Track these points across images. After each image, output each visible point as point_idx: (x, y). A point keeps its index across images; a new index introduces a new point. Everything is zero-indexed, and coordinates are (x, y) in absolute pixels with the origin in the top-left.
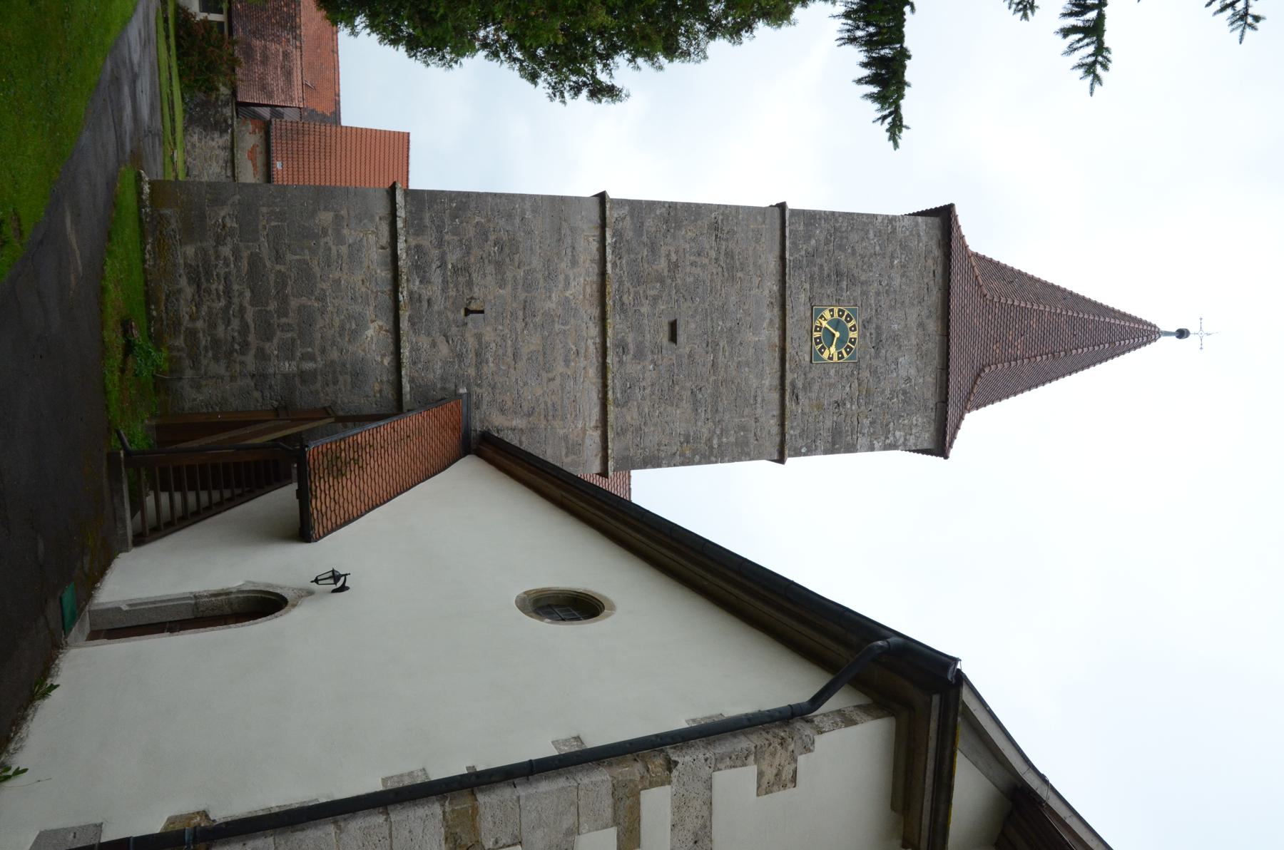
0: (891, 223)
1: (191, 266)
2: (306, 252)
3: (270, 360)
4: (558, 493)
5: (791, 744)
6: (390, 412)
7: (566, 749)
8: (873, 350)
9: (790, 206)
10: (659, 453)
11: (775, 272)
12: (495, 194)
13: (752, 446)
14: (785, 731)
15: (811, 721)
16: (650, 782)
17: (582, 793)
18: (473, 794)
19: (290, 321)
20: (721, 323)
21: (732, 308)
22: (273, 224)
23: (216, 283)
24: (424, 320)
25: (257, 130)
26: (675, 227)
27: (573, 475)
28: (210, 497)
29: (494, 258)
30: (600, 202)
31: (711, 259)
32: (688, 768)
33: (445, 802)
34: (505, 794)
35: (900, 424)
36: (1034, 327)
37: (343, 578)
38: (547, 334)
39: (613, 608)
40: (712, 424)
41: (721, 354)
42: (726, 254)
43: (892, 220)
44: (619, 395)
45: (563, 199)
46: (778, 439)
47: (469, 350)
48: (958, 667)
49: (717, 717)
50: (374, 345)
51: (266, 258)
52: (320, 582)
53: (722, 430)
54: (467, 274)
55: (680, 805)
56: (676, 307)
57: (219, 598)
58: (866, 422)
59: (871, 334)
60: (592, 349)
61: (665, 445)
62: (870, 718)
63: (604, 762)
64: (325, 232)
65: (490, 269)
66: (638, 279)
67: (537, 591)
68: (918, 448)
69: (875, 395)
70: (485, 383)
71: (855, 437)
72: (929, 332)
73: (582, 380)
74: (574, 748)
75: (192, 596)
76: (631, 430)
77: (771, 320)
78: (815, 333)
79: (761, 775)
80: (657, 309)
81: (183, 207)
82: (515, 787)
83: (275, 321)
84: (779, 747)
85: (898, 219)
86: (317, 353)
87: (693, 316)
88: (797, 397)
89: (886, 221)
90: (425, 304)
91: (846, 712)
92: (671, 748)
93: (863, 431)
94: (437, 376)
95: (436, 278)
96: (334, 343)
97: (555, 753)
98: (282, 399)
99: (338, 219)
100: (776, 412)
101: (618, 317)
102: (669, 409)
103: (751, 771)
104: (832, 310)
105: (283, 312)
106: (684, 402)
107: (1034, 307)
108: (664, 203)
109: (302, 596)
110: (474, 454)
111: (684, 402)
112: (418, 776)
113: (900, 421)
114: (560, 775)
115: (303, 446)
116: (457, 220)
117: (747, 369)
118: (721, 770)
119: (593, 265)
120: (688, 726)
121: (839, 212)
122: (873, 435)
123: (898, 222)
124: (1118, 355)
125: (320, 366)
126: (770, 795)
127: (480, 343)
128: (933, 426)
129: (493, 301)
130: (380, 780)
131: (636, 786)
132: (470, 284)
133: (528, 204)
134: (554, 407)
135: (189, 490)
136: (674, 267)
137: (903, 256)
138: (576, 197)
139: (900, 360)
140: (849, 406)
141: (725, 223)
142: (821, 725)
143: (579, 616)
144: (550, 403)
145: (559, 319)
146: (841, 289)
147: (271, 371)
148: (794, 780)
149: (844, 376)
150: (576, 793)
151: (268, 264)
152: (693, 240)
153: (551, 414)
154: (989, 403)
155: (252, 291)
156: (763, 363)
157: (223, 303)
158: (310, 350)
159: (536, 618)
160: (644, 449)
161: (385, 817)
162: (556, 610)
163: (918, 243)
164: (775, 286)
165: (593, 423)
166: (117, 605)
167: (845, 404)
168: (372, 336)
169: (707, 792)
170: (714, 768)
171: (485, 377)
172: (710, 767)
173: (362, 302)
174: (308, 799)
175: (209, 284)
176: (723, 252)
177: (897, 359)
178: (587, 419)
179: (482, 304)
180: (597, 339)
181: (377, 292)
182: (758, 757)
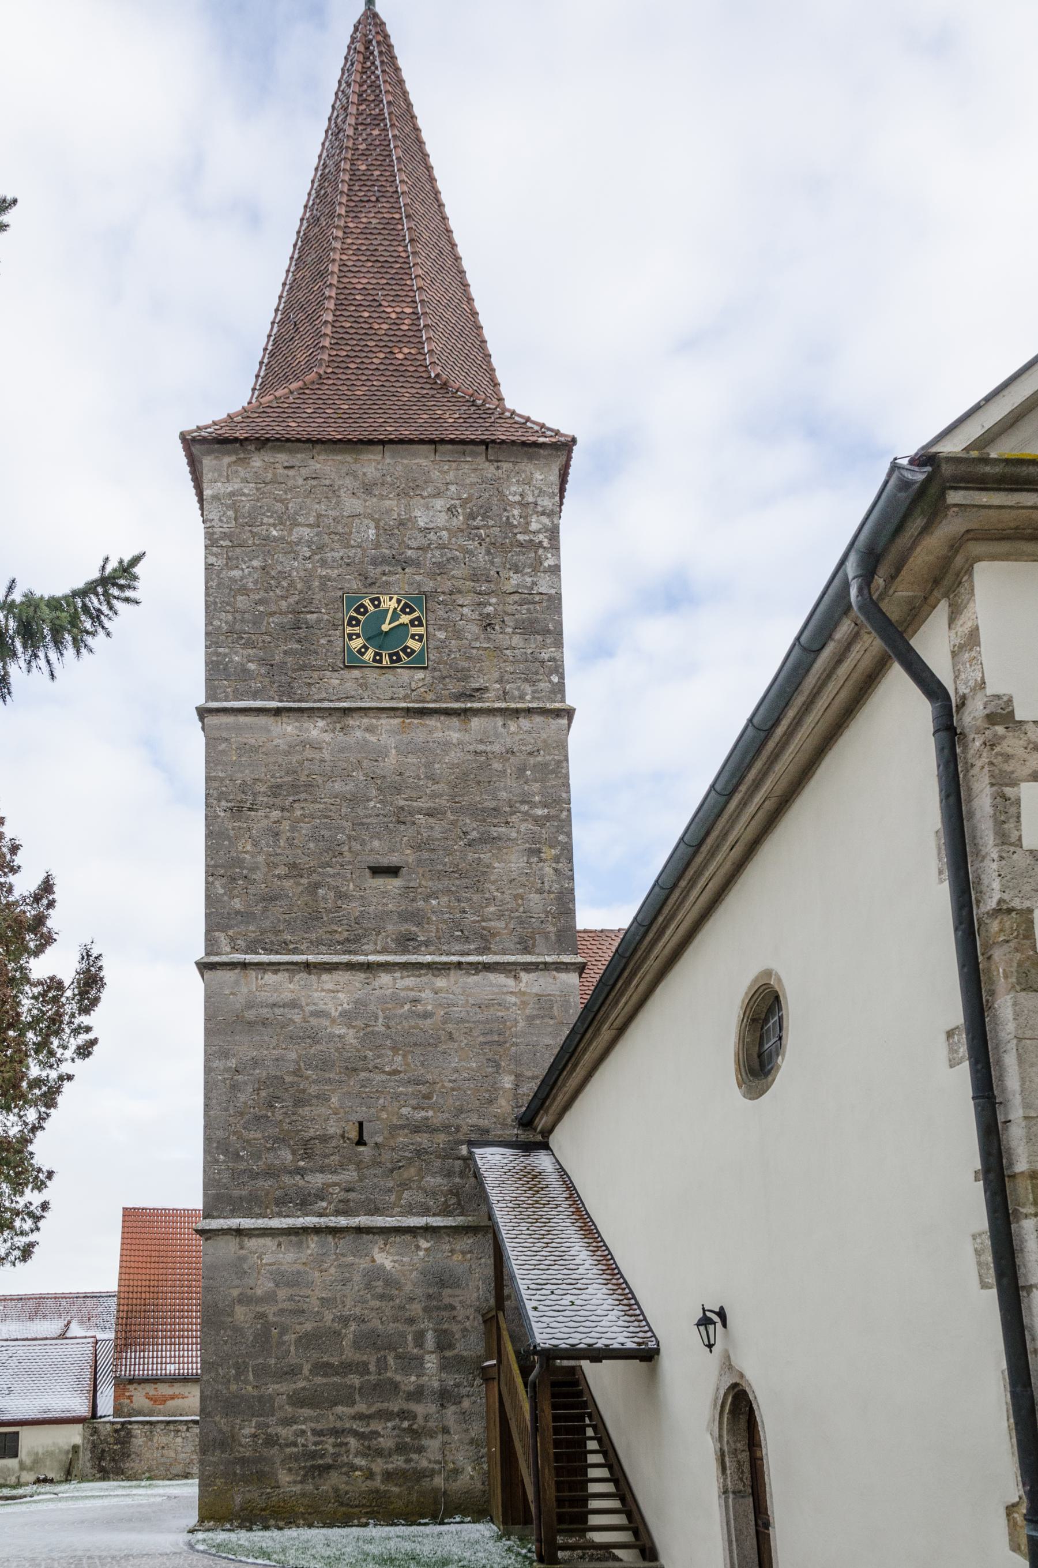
0: (217, 540)
1: (305, 1476)
2: (286, 1338)
3: (423, 1386)
5: (996, 731)
6: (491, 1241)
7: (963, 1050)
8: (406, 570)
9: (201, 700)
11: (297, 724)
13: (547, 758)
14: (974, 739)
16: (1026, 937)
18: (1013, 1176)
20: (372, 804)
21: (351, 787)
22: (251, 1377)
23: (327, 1446)
24: (372, 1196)
25: (127, 1394)
26: (240, 867)
27: (581, 1014)
28: (591, 1438)
29: (290, 1108)
31: (282, 817)
32: (1010, 884)
33: (1021, 1213)
35: (519, 523)
37: (708, 1314)
38: (389, 1041)
39: (768, 973)
40: (515, 816)
41: (415, 804)
42: (275, 795)
43: (212, 541)
44: (472, 947)
47: (411, 1141)
49: (940, 839)
50: (404, 1259)
51: (294, 1386)
52: (712, 1342)
53: (523, 802)
54: (312, 1142)
57: (728, 1464)
58: (515, 579)
59: (384, 574)
60: (410, 981)
61: (543, 883)
63: (987, 1001)
64: (262, 1316)
66: (314, 917)
67: (738, 1070)
68: (557, 491)
69: (474, 565)
70: (455, 1122)
71: (537, 598)
73: (451, 996)
76: (521, 930)
80: (354, 893)
82: (1010, 1121)
83: (373, 1378)
84: (997, 749)
85: (210, 530)
86: (414, 1328)
87: (363, 843)
88: (478, 690)
90: (352, 1195)
91: (957, 642)
93: (529, 585)
95: (317, 1180)
96: (402, 1308)
97: (966, 1065)
99: (244, 1300)
100: (499, 721)
101: (365, 947)
105: (362, 1368)
106: (482, 856)
108: (207, 882)
110: (548, 1137)
111: (482, 856)
113: (515, 523)
114: (999, 1062)
115: (535, 1351)
116: (241, 1154)
117: (437, 766)
118: (1020, 837)
120: (947, 882)
123: (215, 530)
124: (409, 105)
125: (431, 1326)
127: (403, 1127)
129: (347, 1110)
130: (983, 1291)
132: (324, 1139)
133: (216, 1064)
134: (488, 1033)
135: (587, 1506)
136: (295, 870)
137: (265, 520)
138: (206, 1002)
139: (422, 524)
140: (491, 608)
141: (231, 797)
142: (972, 683)
143: (776, 1018)
144: (481, 1039)
145: (370, 1026)
146: (319, 621)
147: (436, 1384)
149: (446, 616)
150: (1028, 1042)
151: (301, 1384)
153: (496, 1038)
155: (336, 1404)
156: (428, 742)
157: (353, 1442)
158: (410, 1338)
160: (547, 913)
162: (766, 1047)
163: (244, 495)
165: (511, 982)
167: (488, 614)
170: (1017, 846)
172: (1014, 852)
173: (349, 1272)
176: (271, 800)
177: (420, 530)
178: (505, 990)
179: (351, 1123)
180: (395, 975)
181: (335, 1254)
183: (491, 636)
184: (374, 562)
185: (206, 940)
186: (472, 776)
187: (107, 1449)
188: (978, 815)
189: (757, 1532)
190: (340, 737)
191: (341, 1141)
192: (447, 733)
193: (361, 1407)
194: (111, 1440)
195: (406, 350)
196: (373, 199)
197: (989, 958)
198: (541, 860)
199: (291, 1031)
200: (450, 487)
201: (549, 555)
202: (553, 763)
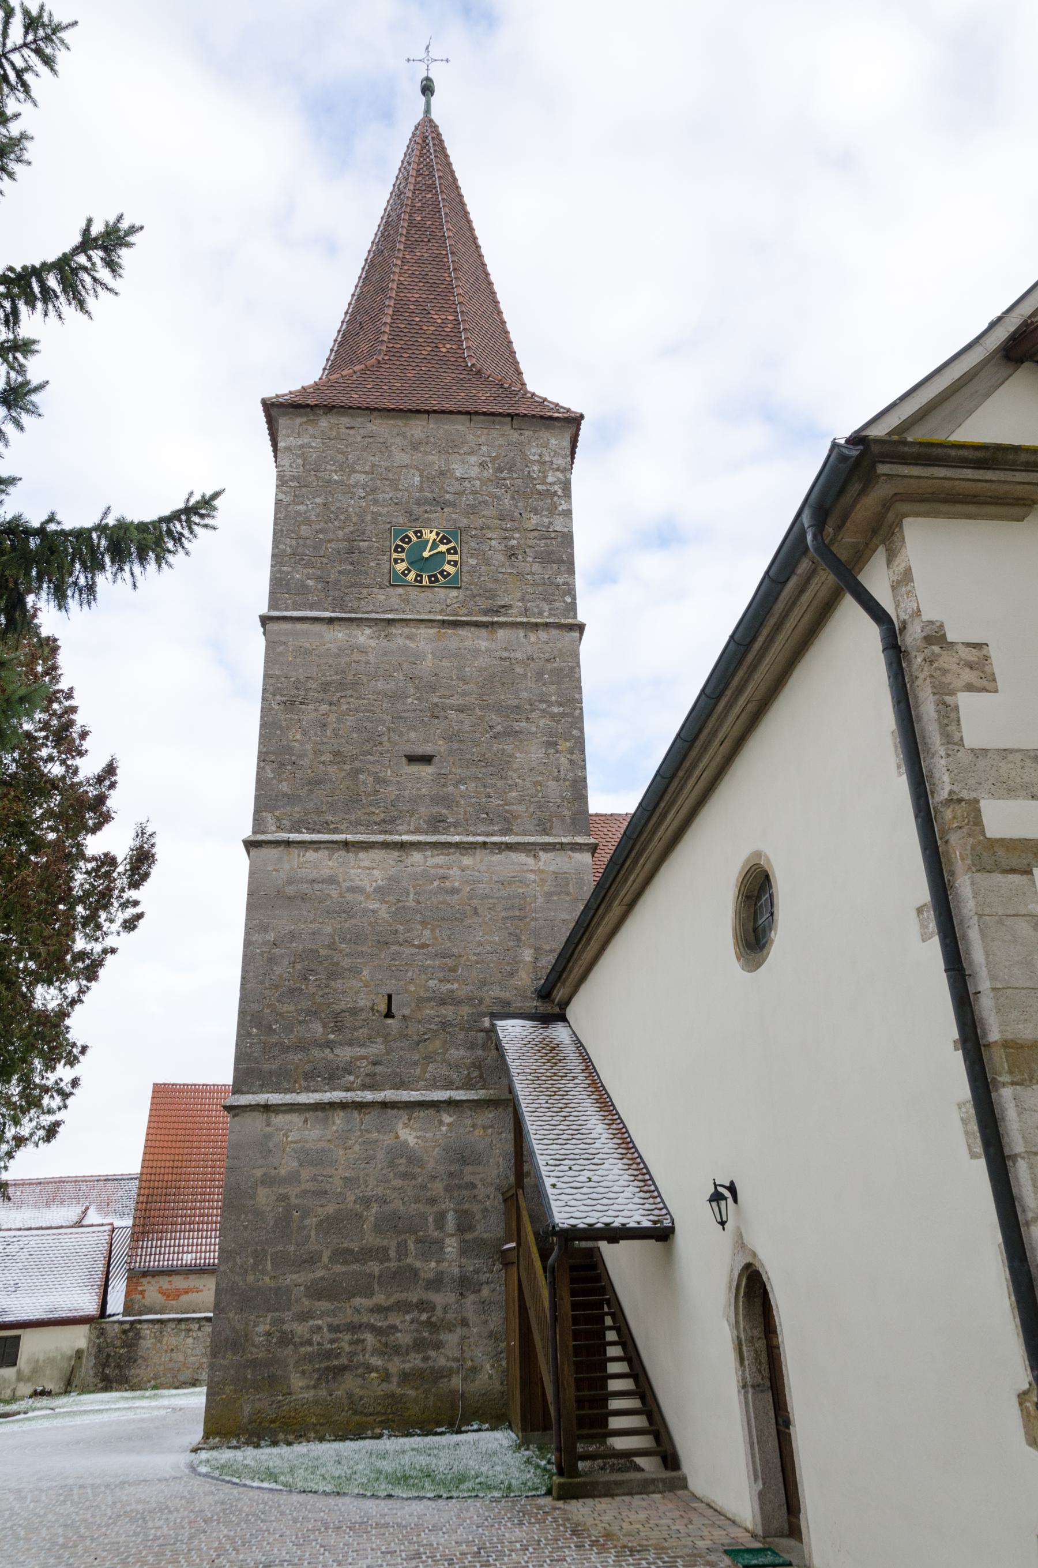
0: (287, 481)
1: (319, 1379)
2: (307, 1222)
3: (442, 1272)
4: (617, 910)
6: (511, 1115)
7: (932, 926)
9: (264, 610)
10: (568, 780)
11: (347, 631)
12: (243, 978)
14: (916, 656)
15: (904, 623)
17: (987, 911)
19: (393, 1244)
20: (410, 700)
21: (392, 685)
22: (269, 1266)
23: (343, 1344)
24: (398, 1070)
25: (140, 1288)
26: (289, 754)
28: (613, 1343)
29: (323, 981)
30: (257, 847)
31: (330, 710)
33: (999, 1082)
34: (986, 1006)
35: (538, 476)
36: (418, 296)
37: (720, 1189)
38: (419, 916)
39: (758, 854)
41: (448, 701)
42: (325, 692)
43: (282, 482)
44: (496, 828)
45: (251, 894)
46: (554, 632)
47: (436, 1014)
48: (842, 441)
50: (427, 1135)
51: (312, 1276)
52: (724, 1219)
53: (541, 701)
54: (343, 1015)
55: (1008, 790)
56: (389, 755)
58: (535, 520)
59: (426, 512)
60: (440, 860)
62: (903, 550)
63: (949, 880)
65: (338, 984)
67: (737, 944)
68: (569, 453)
69: (501, 508)
72: (424, 436)
74: (930, 915)
75: (743, 1391)
77: (408, 637)
78: (424, 583)
79: (970, 688)
80: (392, 778)
81: (241, 1391)
83: (392, 1265)
84: (935, 665)
85: (282, 473)
86: (435, 1209)
87: (401, 735)
88: (503, 607)
89: (284, 488)
90: (379, 1069)
91: (895, 578)
92: (933, 797)
93: (546, 524)
94: (468, 1055)
95: (346, 1053)
96: (424, 1187)
98: (493, 1257)
99: (267, 1181)
100: (521, 633)
102: (515, 766)
103: (965, 700)
104: (396, 561)
107: (394, 296)
108: (259, 767)
109: (743, 1243)
110: (565, 1009)
112: (967, 1112)
113: (535, 476)
114: (964, 936)
116: (274, 1027)
117: (467, 669)
119: (334, 857)
121: (273, 548)
122: (553, 509)
123: (286, 473)
125: (452, 1206)
126: (996, 676)
127: (429, 999)
128: (541, 434)
129: (377, 982)
131: (979, 842)
132: (355, 1011)
134: (509, 909)
137: (328, 467)
138: (250, 877)
139: (458, 475)
140: (515, 542)
141: (285, 693)
142: (909, 611)
143: (768, 895)
146: (370, 548)
147: (456, 1271)
148: (978, 646)
149: (477, 547)
150: (987, 918)
151: (320, 1273)
152: (305, 733)
153: (517, 913)
154: (514, 357)
155: (354, 1296)
158: (431, 1219)
159: (770, 949)
160: (563, 798)
161: (1019, 1159)
162: (760, 922)
163: (312, 447)
164: (365, 632)
165: (530, 861)
166: (756, 1498)
167: (513, 546)
168: (417, 1137)
169: (990, 754)
170: (960, 745)
171: (471, 994)
172: (958, 751)
173: (373, 1149)
174: (999, 1258)
175: (343, 1354)
176: (321, 696)
177: (457, 479)
178: (525, 868)
179: (380, 996)
180: (426, 853)
181: (360, 1130)
182: (946, 690)
183: (515, 564)
184: (418, 503)
185: (255, 819)
186: (498, 678)
187: (112, 1354)
188: (925, 719)
189: (778, 1432)
190: (384, 643)
191: (371, 1014)
192: (476, 642)
193: (380, 1298)
194: (118, 1343)
195: (448, 346)
196: (426, 240)
197: (947, 842)
198: (557, 752)
199: (328, 906)
200: (482, 447)
201: (563, 502)
202: (567, 668)
